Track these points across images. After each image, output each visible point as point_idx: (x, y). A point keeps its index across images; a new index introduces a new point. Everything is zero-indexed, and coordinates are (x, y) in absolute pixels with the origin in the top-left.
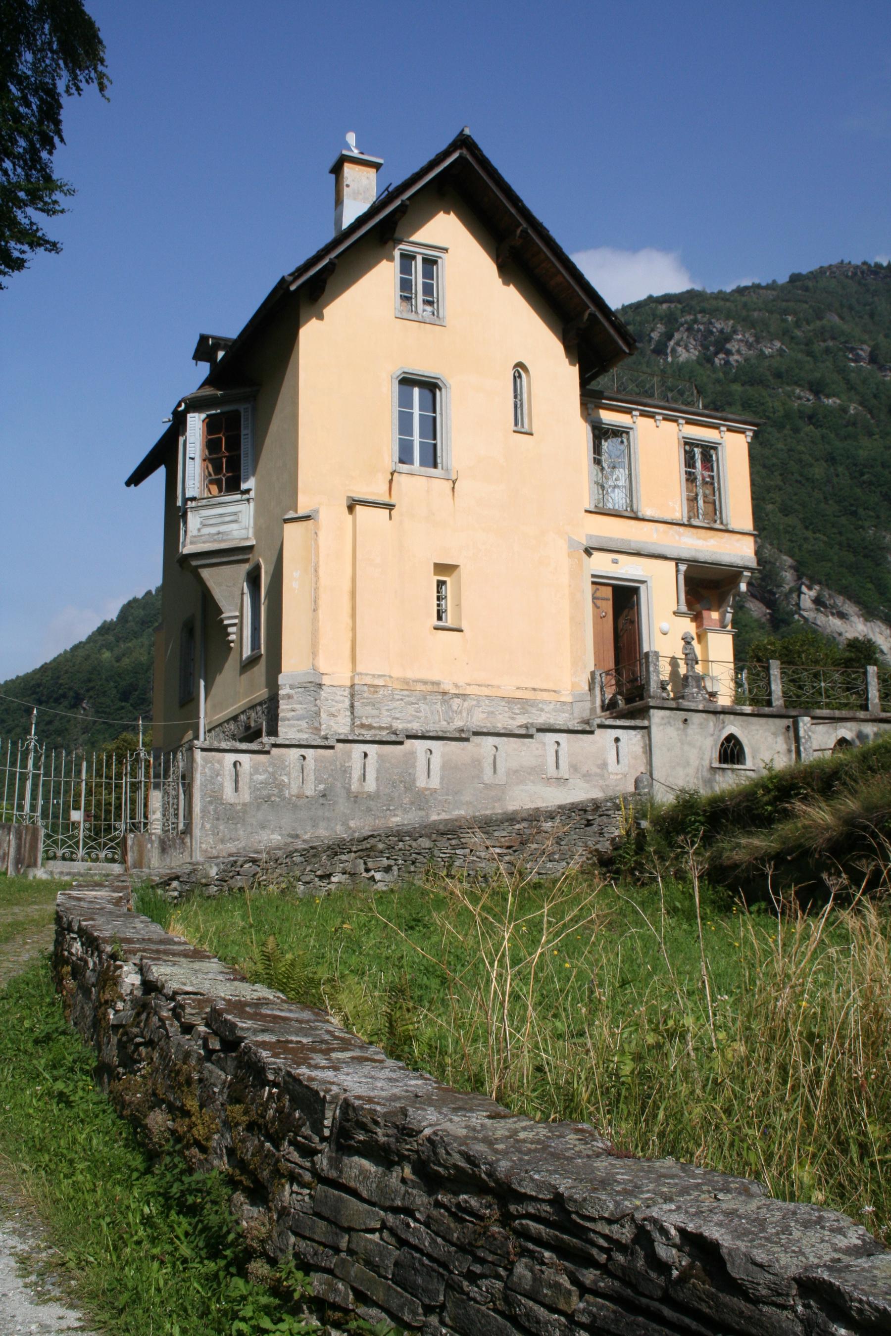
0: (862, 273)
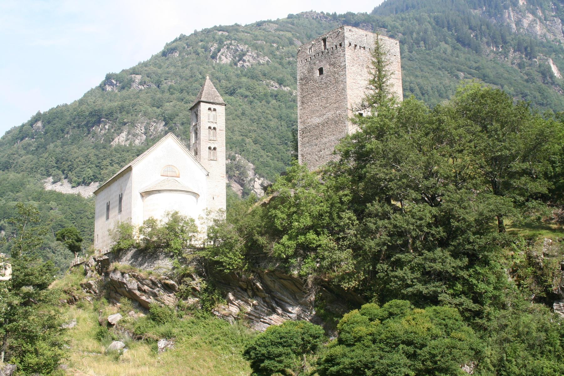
0: (320, 17)
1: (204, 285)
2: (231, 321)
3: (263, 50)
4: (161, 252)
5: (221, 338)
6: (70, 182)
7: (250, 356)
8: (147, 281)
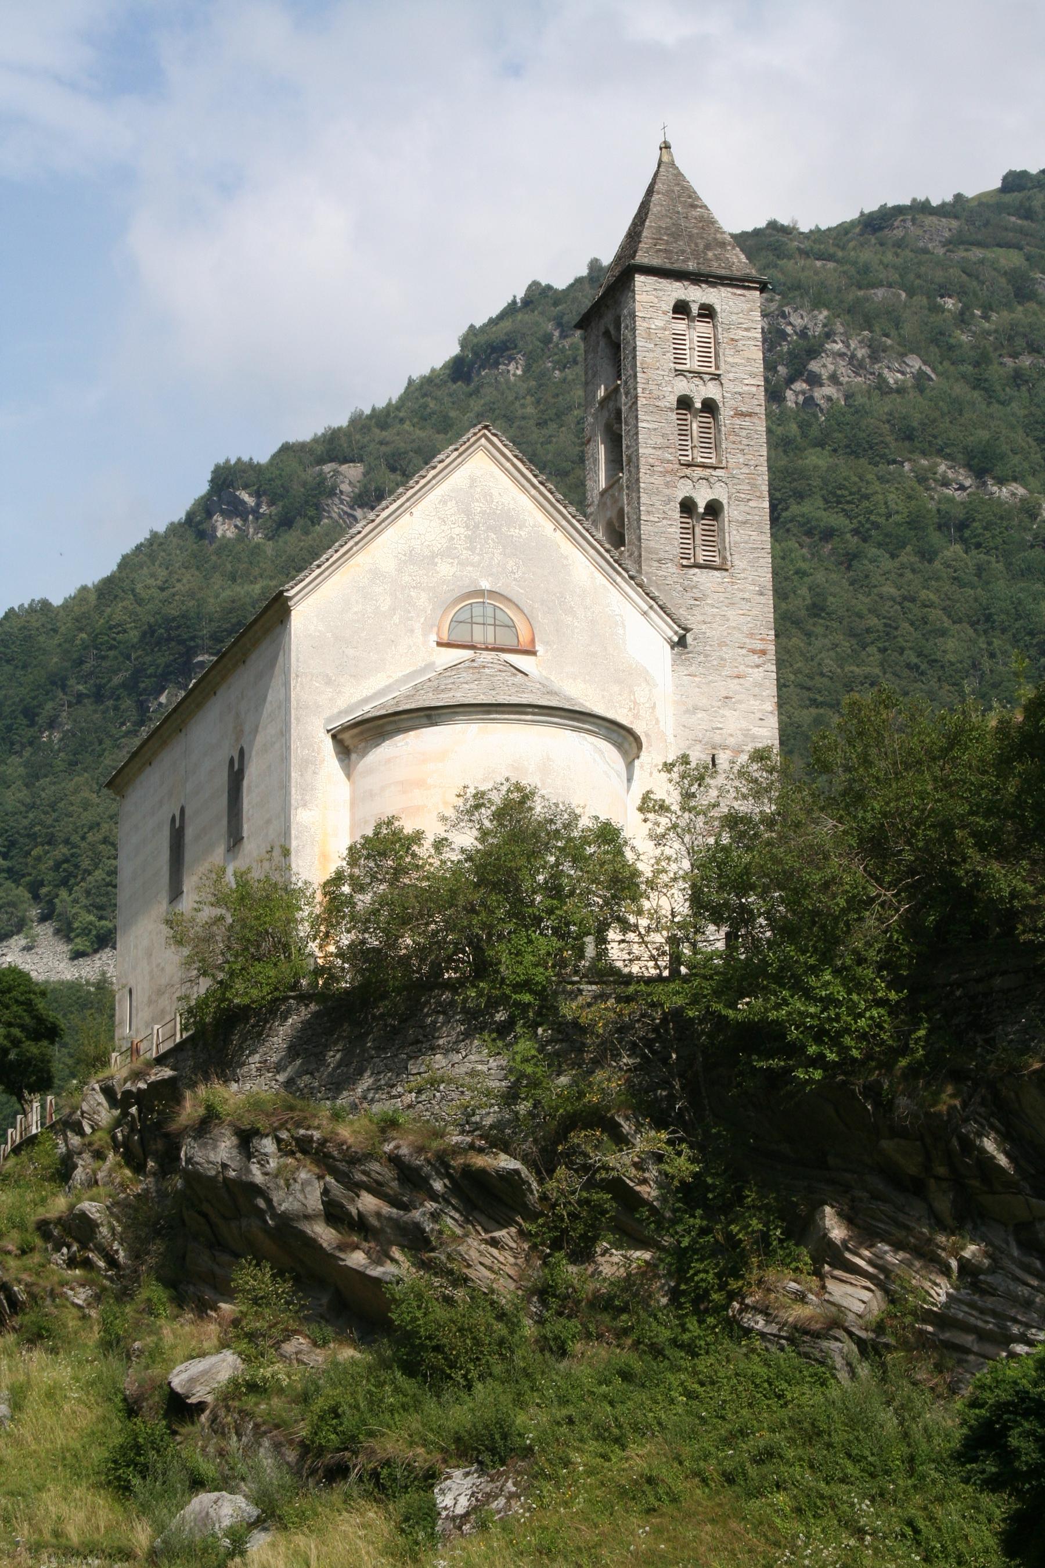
1: (683, 1165)
2: (839, 1362)
3: (897, 327)
4: (445, 1009)
5: (790, 1454)
6: (65, 932)
7: (1007, 1456)
8: (375, 1166)
